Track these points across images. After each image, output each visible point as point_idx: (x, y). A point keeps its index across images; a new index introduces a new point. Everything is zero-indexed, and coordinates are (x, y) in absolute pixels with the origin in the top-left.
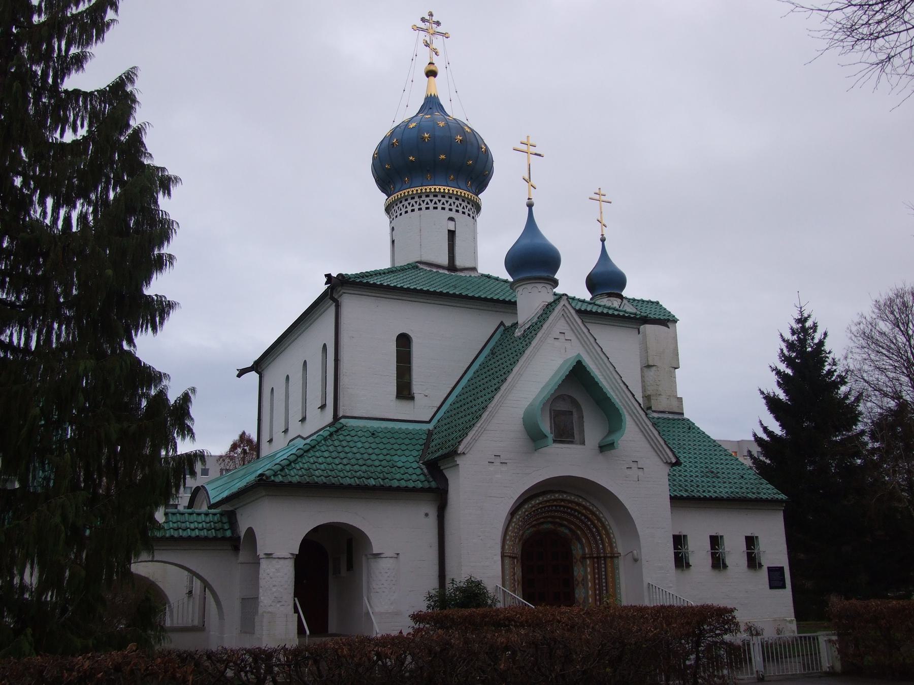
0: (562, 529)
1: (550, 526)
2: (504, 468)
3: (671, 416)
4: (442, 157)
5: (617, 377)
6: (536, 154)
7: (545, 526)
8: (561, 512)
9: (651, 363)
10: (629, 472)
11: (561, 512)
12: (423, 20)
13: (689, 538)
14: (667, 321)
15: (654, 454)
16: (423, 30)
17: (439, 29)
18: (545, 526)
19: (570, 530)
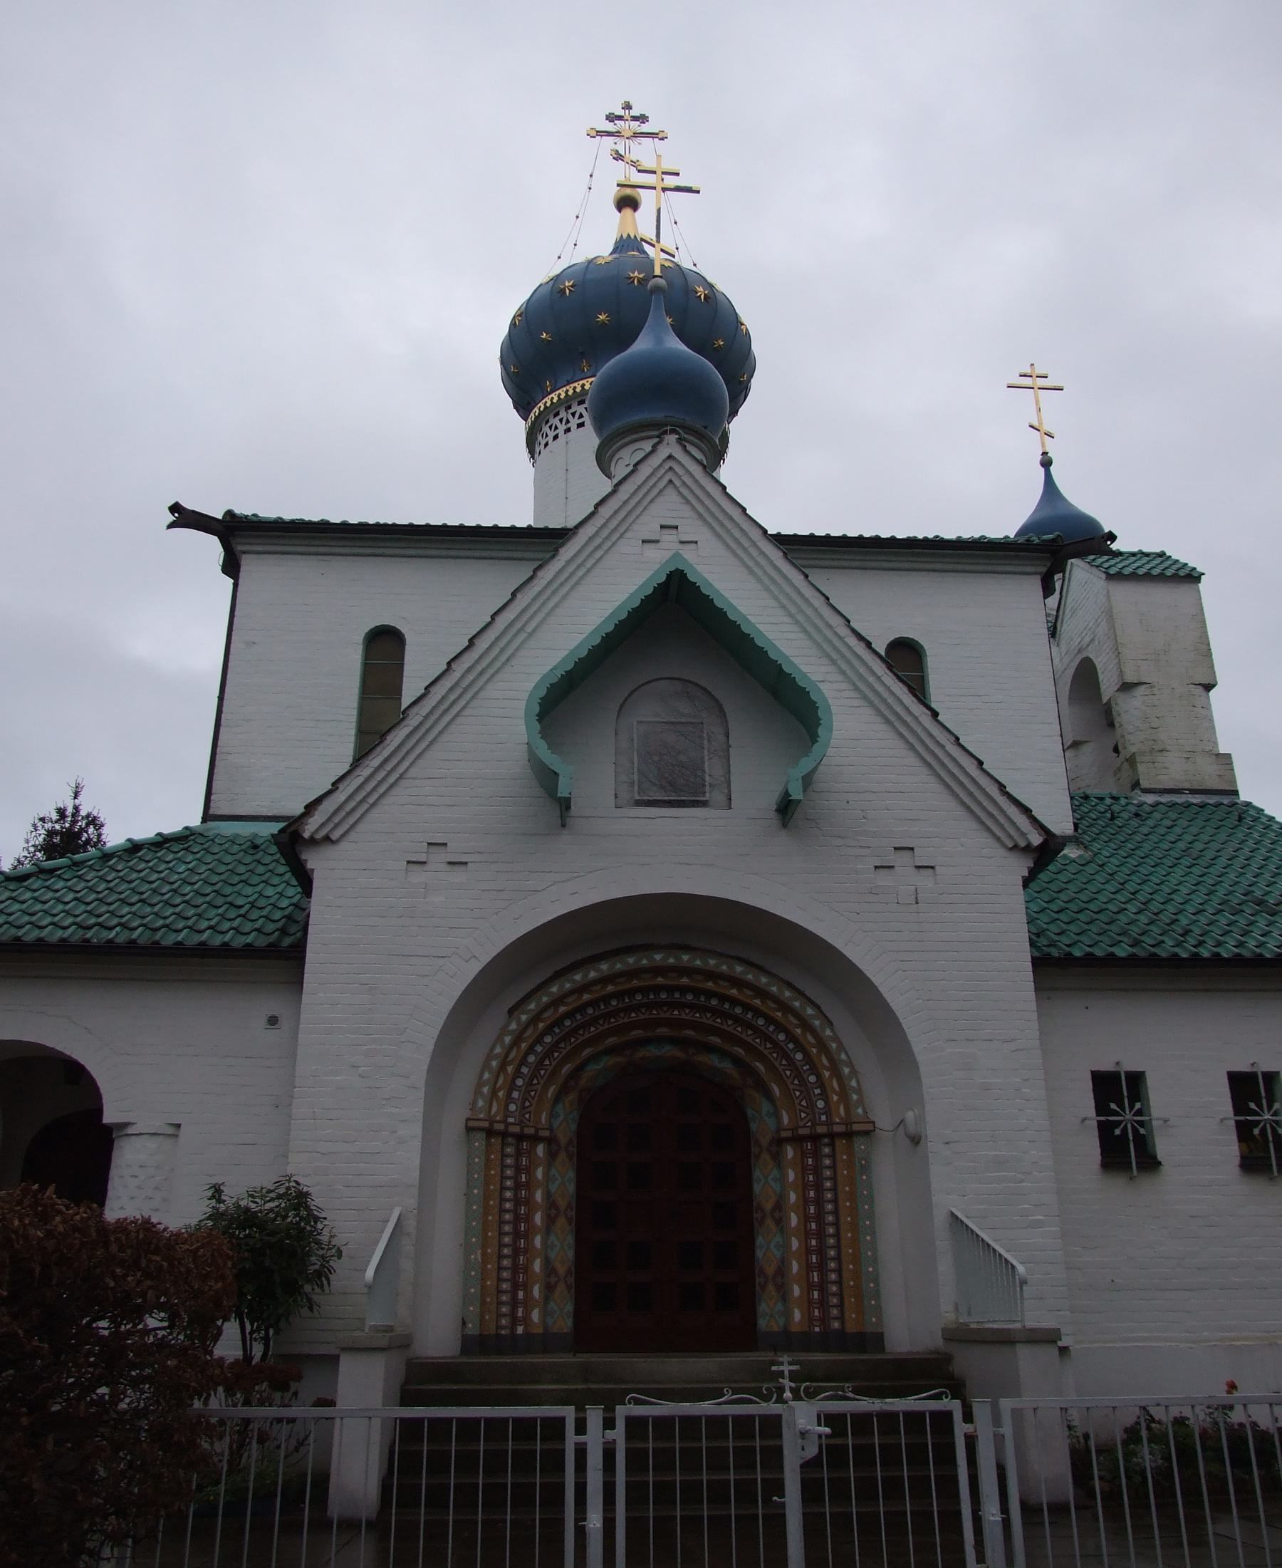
0: (714, 1060)
1: (668, 1050)
2: (458, 876)
3: (1196, 799)
4: (602, 317)
5: (836, 621)
6: (678, 189)
7: (653, 1051)
8: (692, 1007)
9: (1130, 678)
10: (883, 879)
11: (692, 1007)
12: (612, 118)
13: (1151, 1082)
14: (1192, 577)
15: (974, 825)
16: (609, 134)
17: (645, 128)
18: (714, 1060)
19: (736, 1061)
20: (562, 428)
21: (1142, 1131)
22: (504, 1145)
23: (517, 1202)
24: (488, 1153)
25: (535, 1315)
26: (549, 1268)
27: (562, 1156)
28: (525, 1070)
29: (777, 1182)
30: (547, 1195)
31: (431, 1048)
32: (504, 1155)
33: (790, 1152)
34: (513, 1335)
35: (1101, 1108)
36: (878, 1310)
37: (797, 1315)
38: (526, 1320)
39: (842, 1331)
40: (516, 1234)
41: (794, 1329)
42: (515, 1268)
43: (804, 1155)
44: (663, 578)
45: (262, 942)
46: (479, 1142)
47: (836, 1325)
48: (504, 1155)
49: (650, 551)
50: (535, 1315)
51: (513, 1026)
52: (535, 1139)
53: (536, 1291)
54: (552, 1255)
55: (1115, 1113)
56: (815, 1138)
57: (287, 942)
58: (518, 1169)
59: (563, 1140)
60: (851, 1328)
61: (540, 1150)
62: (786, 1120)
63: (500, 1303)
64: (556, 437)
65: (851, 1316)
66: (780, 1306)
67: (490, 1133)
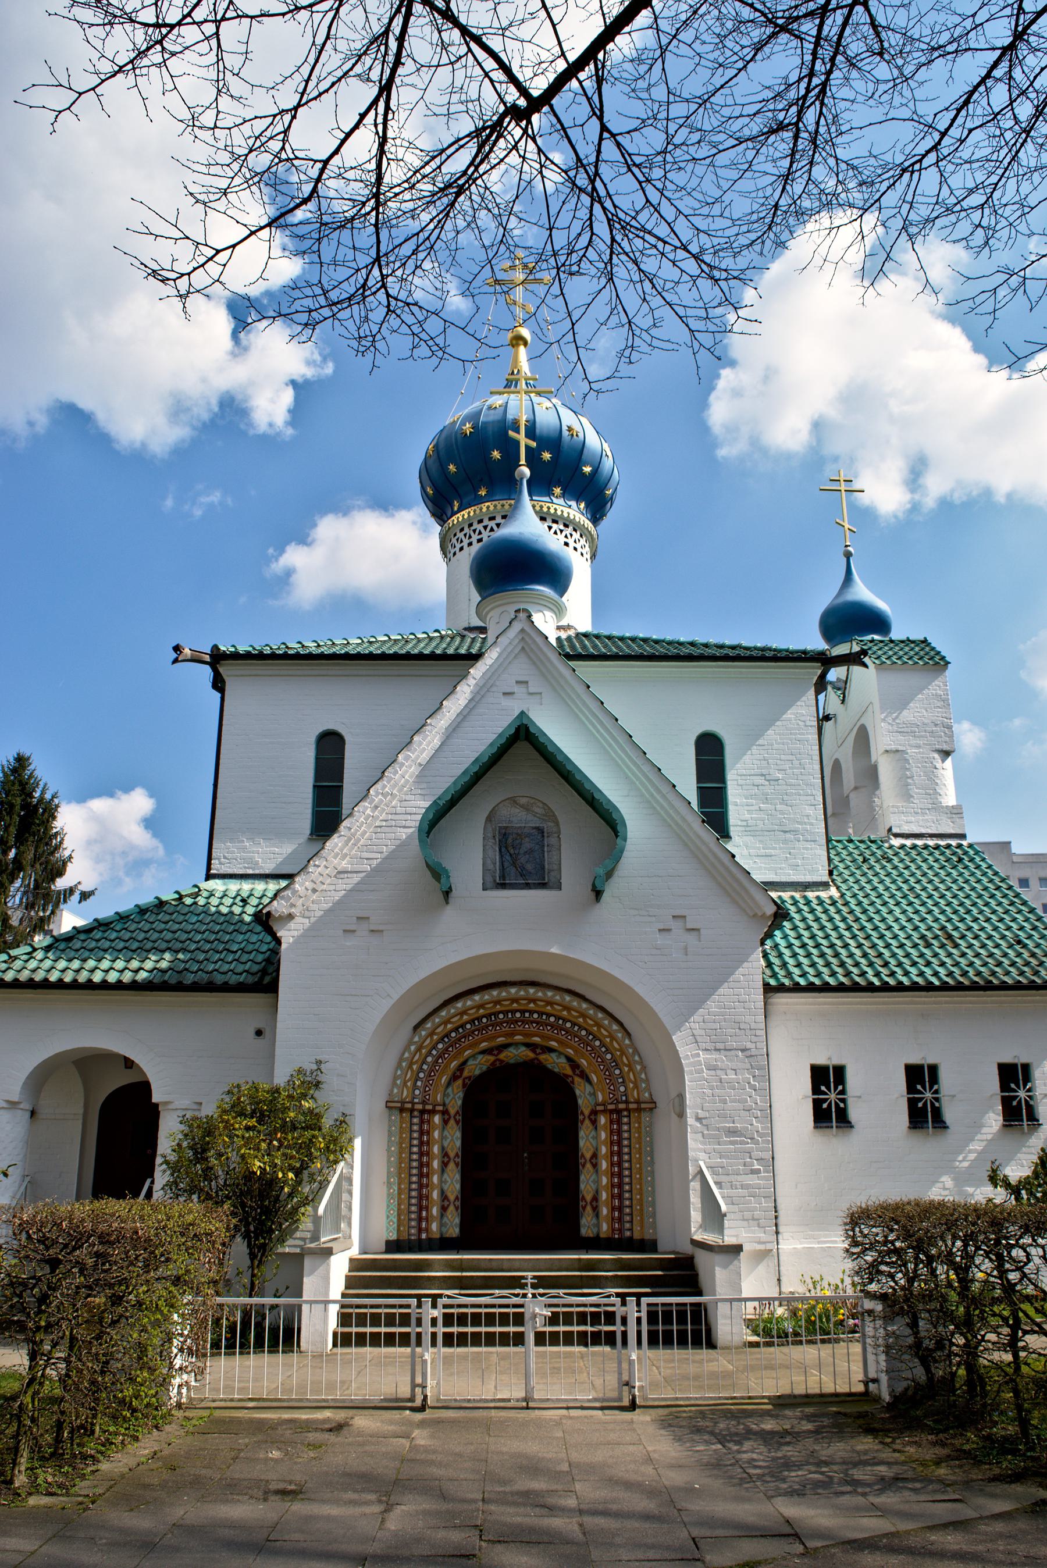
20: (466, 541)
21: (842, 1105)
22: (412, 1117)
23: (421, 1154)
24: (401, 1123)
25: (434, 1227)
26: (444, 1197)
27: (452, 1122)
28: (434, 1052)
29: (592, 1139)
30: (443, 1149)
31: (378, 1021)
32: (412, 1124)
33: (602, 1120)
34: (420, 1239)
35: (816, 1090)
36: (654, 1225)
37: (605, 1227)
38: (427, 1230)
39: (631, 1238)
40: (421, 1175)
41: (602, 1236)
42: (420, 1197)
43: (611, 1122)
44: (513, 731)
45: (251, 980)
46: (395, 1117)
47: (628, 1234)
48: (412, 1124)
49: (506, 702)
50: (434, 1227)
51: (416, 1039)
52: (433, 1112)
53: (435, 1211)
54: (445, 1188)
55: (825, 1093)
56: (619, 1112)
57: (267, 979)
58: (422, 1133)
59: (452, 1112)
60: (637, 1236)
61: (437, 1119)
62: (600, 1098)
63: (410, 1220)
64: (461, 549)
65: (637, 1228)
66: (594, 1221)
67: (402, 1110)
